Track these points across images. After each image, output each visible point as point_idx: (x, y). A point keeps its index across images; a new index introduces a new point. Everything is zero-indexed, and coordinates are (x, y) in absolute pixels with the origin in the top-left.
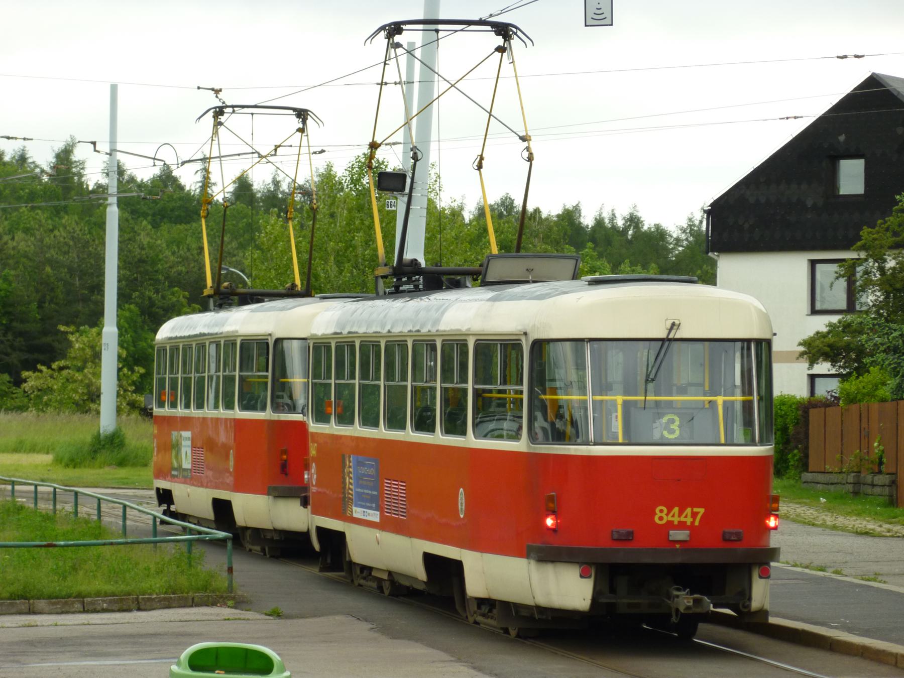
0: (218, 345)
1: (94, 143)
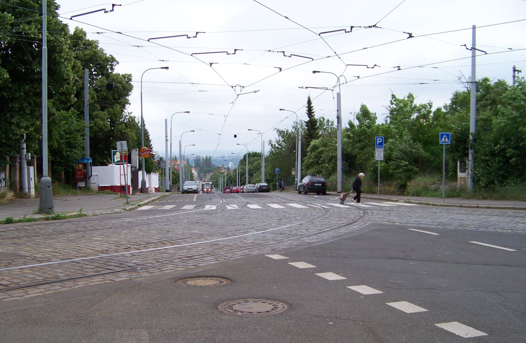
0: (114, 162)
1: (284, 52)
